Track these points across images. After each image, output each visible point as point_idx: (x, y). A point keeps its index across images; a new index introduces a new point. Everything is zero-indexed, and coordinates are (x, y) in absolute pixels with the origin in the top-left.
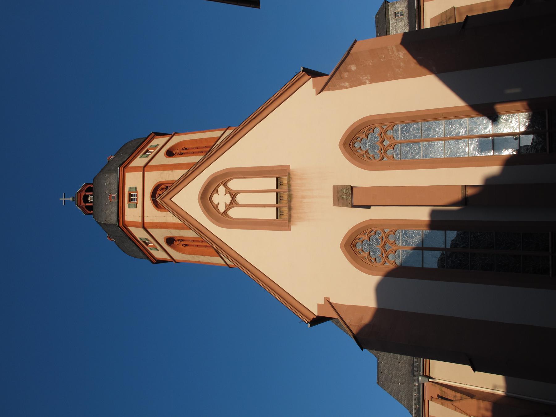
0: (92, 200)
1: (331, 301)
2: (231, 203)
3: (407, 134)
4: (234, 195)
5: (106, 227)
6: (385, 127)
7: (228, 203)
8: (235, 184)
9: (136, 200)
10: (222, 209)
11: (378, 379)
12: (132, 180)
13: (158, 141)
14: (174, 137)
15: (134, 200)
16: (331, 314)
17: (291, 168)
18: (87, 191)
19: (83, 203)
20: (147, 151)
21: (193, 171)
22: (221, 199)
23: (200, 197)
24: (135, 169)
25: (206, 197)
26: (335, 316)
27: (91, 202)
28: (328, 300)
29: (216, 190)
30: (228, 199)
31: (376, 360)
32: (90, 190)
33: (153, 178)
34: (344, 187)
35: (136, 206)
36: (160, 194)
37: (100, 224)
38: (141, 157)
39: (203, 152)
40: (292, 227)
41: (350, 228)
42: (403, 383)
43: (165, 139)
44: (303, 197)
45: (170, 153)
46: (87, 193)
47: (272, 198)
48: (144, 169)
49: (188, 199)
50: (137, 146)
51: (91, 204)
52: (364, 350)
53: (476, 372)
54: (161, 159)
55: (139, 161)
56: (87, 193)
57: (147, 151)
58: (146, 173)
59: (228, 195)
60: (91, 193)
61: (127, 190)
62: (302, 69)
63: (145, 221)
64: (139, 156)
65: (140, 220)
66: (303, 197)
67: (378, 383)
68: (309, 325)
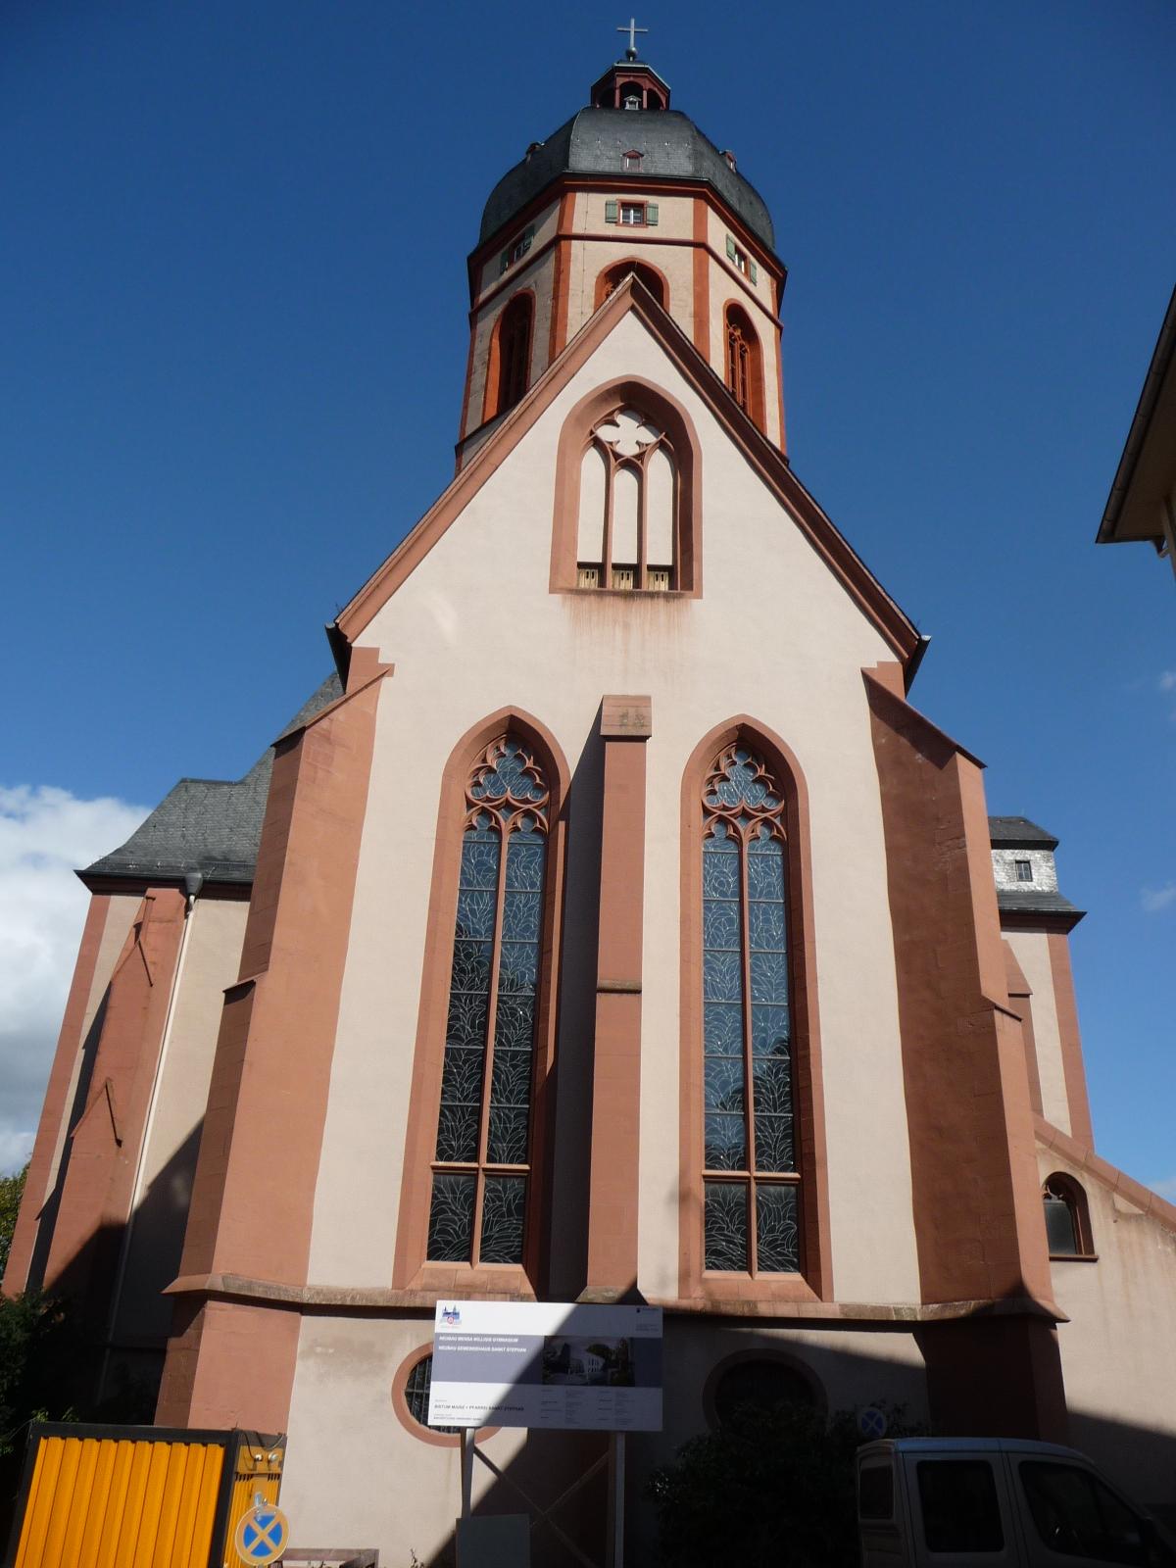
0: (628, 106)
1: (386, 680)
2: (617, 456)
3: (760, 869)
4: (634, 465)
5: (561, 140)
6: (777, 821)
7: (618, 449)
8: (659, 468)
9: (626, 223)
10: (605, 433)
11: (193, 781)
12: (674, 214)
13: (763, 285)
14: (772, 326)
15: (626, 217)
16: (354, 680)
17: (695, 602)
18: (651, 93)
19: (620, 81)
20: (743, 257)
21: (688, 358)
22: (628, 434)
23: (624, 381)
24: (700, 223)
25: (636, 398)
26: (351, 687)
27: (623, 104)
28: (387, 671)
29: (647, 421)
30: (629, 450)
31: (237, 780)
32: (654, 103)
33: (675, 267)
34: (643, 720)
35: (609, 220)
36: (640, 286)
37: (570, 124)
38: (728, 237)
39: (734, 386)
40: (557, 597)
41: (541, 733)
42: (183, 836)
43: (769, 303)
44: (626, 626)
45: (735, 315)
46: (645, 93)
47: (623, 552)
48: (700, 245)
49: (630, 352)
50: (753, 241)
51: (617, 104)
52: (274, 749)
53: (224, 995)
54: (722, 291)
55: (719, 235)
56: (645, 93)
57: (743, 257)
58: (690, 249)
59: (636, 450)
60: (645, 106)
61: (651, 199)
62: (926, 638)
63: (574, 243)
64: (731, 235)
65: (577, 230)
66: (626, 626)
67: (184, 781)
68: (332, 626)
